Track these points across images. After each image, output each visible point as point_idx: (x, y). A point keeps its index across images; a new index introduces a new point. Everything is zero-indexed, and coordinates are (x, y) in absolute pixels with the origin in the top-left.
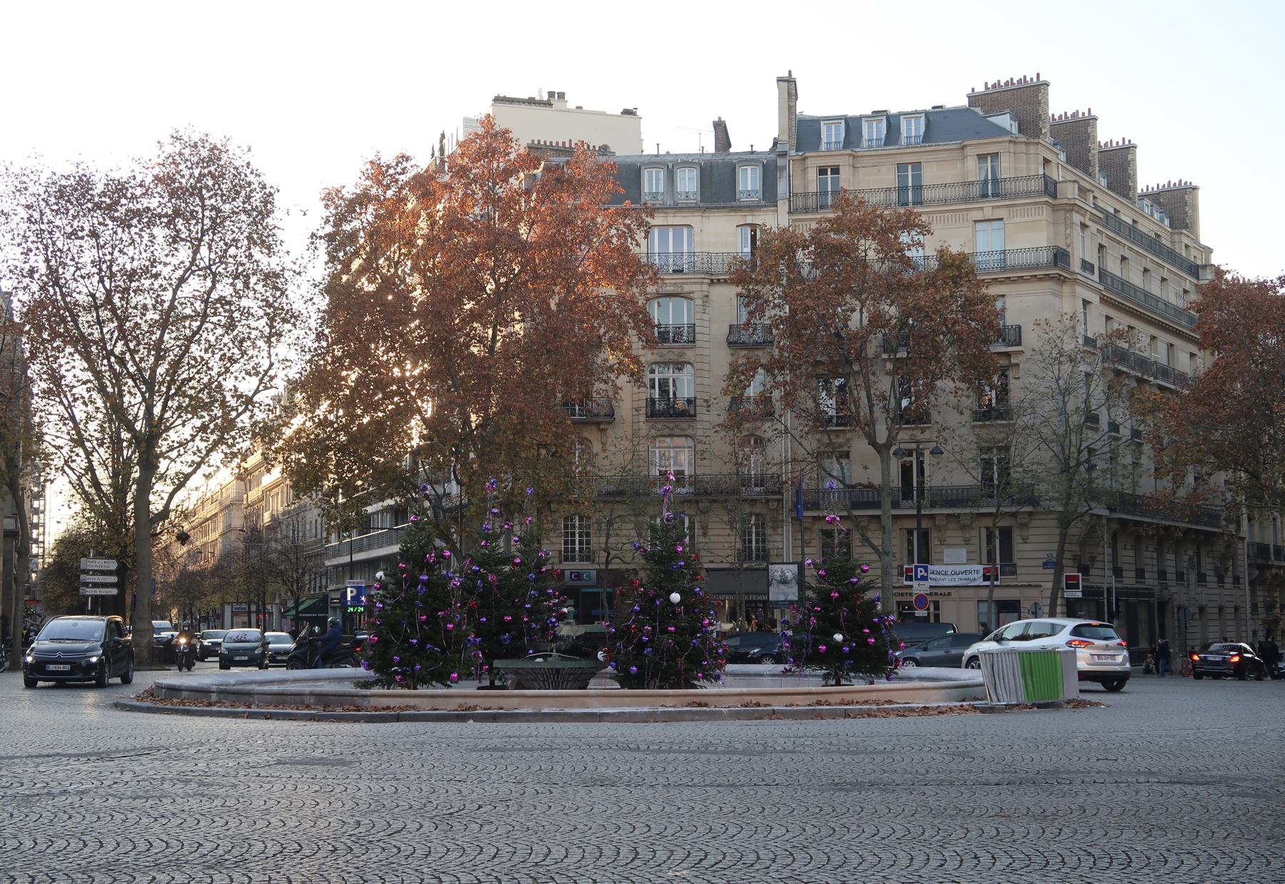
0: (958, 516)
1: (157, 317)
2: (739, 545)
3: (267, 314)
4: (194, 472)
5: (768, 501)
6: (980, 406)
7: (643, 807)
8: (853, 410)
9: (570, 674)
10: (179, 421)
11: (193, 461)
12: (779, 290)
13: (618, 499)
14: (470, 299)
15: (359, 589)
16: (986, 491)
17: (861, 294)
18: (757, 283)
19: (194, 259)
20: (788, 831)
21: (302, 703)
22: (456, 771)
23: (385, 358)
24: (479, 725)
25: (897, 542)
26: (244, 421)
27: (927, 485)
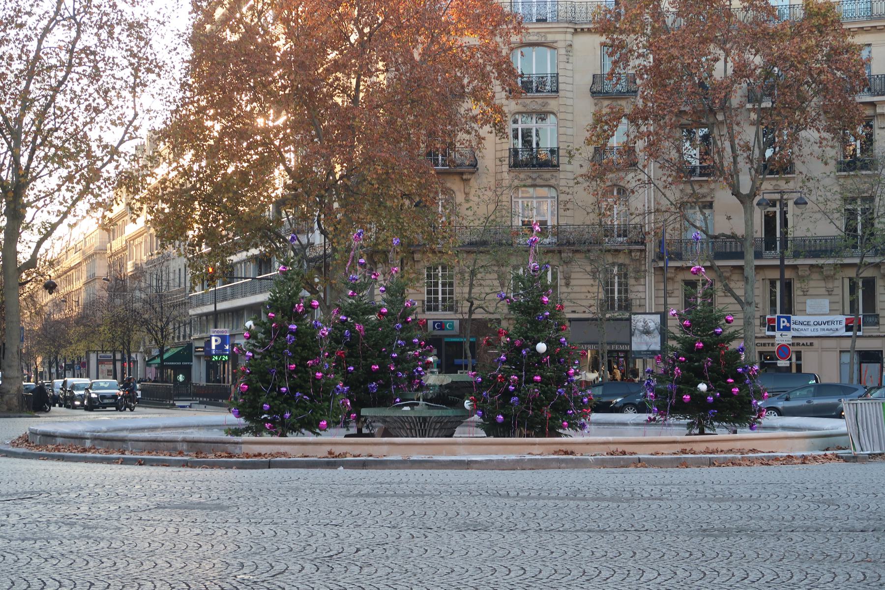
0: (821, 267)
1: (22, 67)
2: (602, 296)
3: (131, 64)
4: (61, 221)
5: (630, 251)
6: (845, 157)
7: (516, 551)
8: (718, 161)
9: (437, 423)
10: (46, 171)
11: (59, 211)
12: (643, 39)
13: (481, 249)
14: (333, 49)
15: (223, 338)
16: (851, 242)
17: (725, 43)
18: (622, 32)
19: (58, 9)
20: (659, 574)
21: (175, 449)
22: (332, 516)
23: (248, 109)
24: (350, 472)
25: (759, 293)
26: (110, 171)
27: (790, 236)
